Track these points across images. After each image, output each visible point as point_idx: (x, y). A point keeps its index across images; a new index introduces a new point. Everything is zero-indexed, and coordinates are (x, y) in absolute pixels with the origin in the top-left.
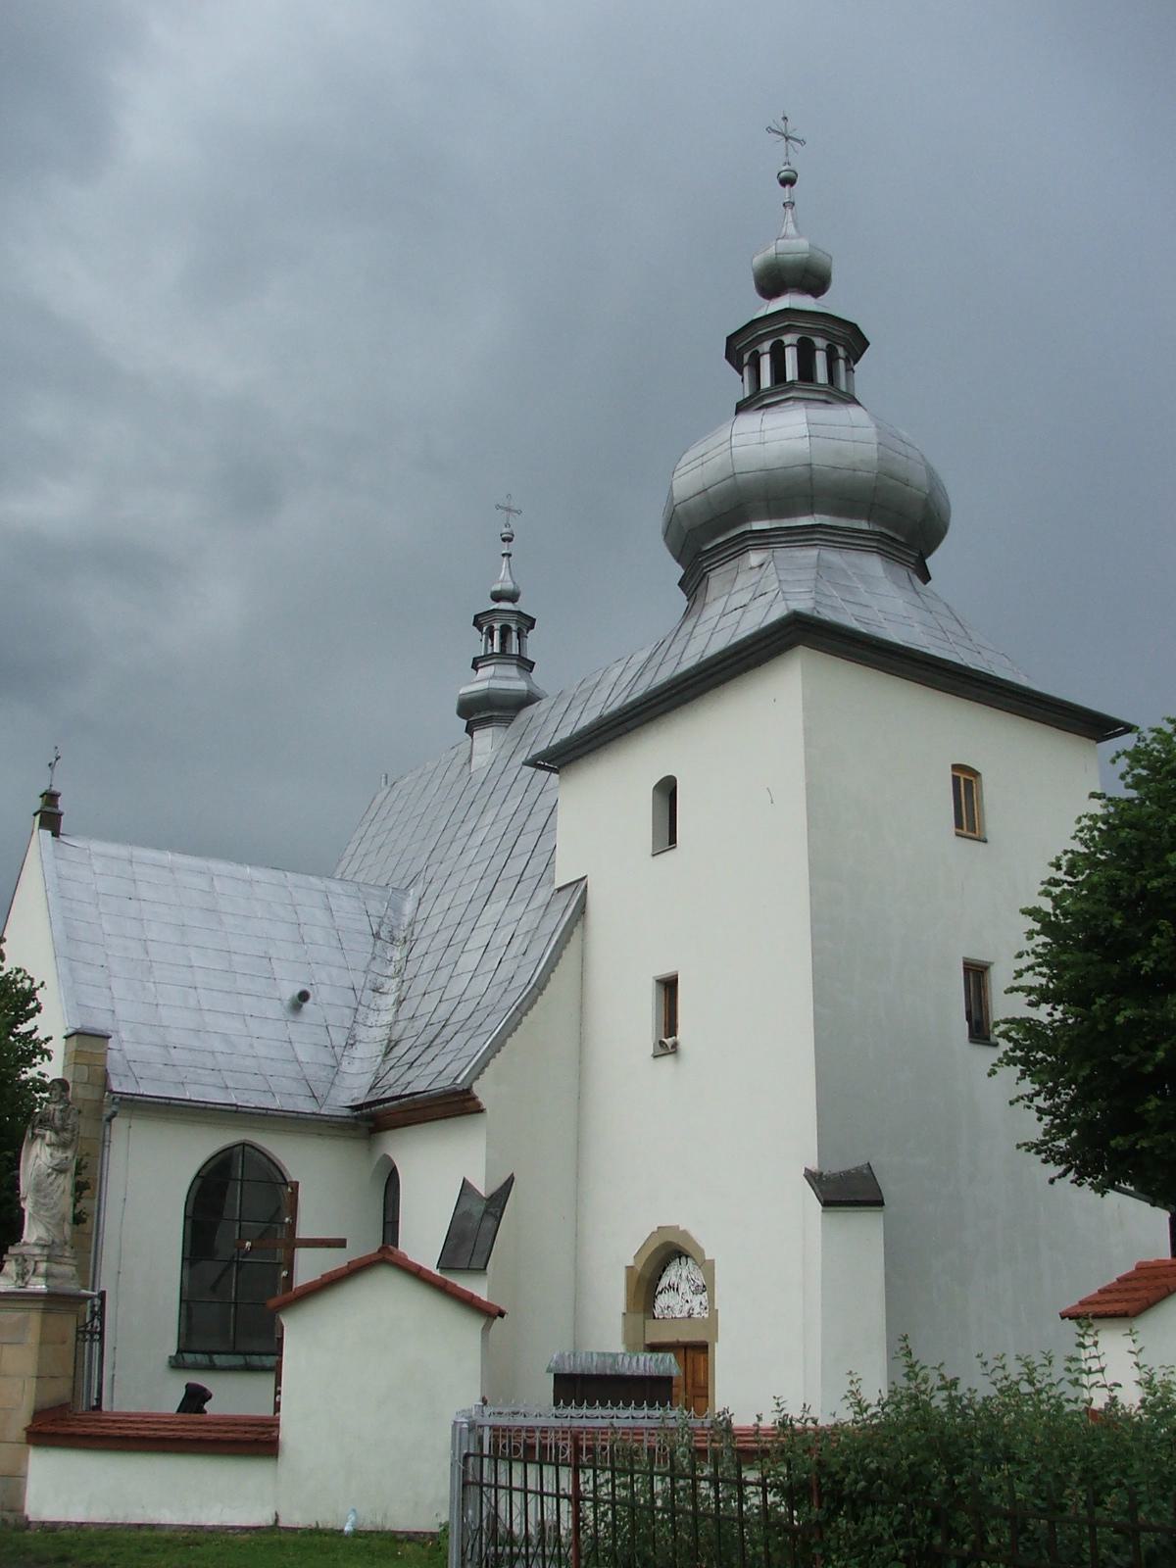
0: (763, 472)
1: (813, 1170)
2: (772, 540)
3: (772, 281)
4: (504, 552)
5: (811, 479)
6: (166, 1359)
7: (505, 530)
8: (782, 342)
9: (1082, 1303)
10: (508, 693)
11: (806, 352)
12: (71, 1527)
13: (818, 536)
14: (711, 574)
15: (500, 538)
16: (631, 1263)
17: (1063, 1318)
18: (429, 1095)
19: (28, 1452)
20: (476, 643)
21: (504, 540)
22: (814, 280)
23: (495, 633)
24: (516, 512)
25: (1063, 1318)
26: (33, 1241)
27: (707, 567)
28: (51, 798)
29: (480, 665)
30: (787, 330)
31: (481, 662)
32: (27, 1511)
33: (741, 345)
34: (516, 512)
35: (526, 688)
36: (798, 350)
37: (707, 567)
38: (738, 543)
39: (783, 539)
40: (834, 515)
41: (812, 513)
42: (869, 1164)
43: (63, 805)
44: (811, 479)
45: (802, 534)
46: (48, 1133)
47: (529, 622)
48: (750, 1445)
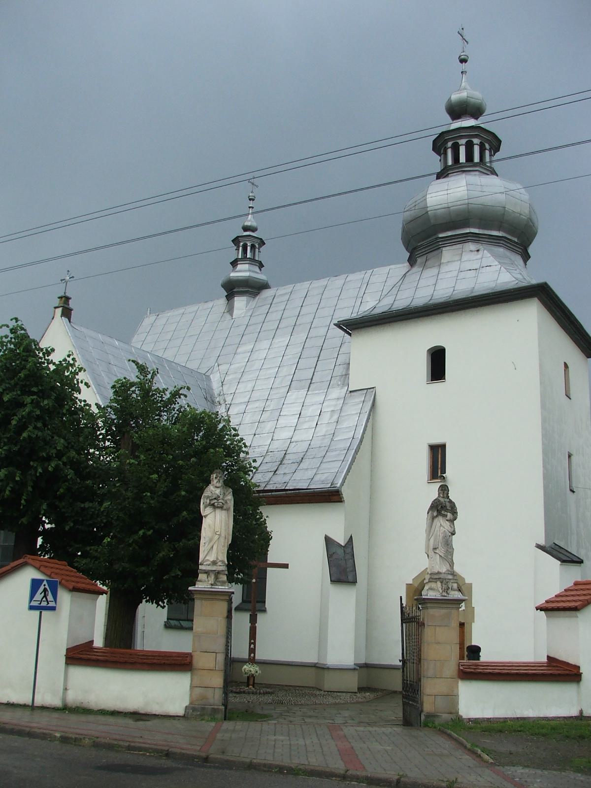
0: (482, 206)
1: (542, 545)
2: (481, 239)
3: (457, 110)
4: (250, 206)
5: (504, 214)
6: (163, 623)
7: (251, 194)
8: (472, 141)
9: (547, 602)
10: (258, 280)
11: (469, 147)
12: (484, 721)
13: (469, 238)
14: (444, 249)
15: (248, 199)
16: (411, 582)
17: (537, 609)
18: (314, 491)
19: (458, 682)
20: (234, 253)
21: (250, 200)
22: (476, 111)
23: (248, 247)
24: (256, 186)
25: (537, 609)
26: (444, 572)
27: (441, 245)
28: (66, 299)
29: (239, 263)
30: (476, 136)
31: (240, 261)
32: (460, 713)
33: (447, 138)
34: (256, 186)
35: (266, 279)
36: (466, 147)
37: (441, 245)
38: (465, 237)
39: (486, 240)
40: (482, 229)
41: (499, 231)
42: (554, 543)
43: (72, 304)
44: (504, 214)
45: (494, 239)
46: (449, 514)
47: (262, 243)
48: (521, 671)
